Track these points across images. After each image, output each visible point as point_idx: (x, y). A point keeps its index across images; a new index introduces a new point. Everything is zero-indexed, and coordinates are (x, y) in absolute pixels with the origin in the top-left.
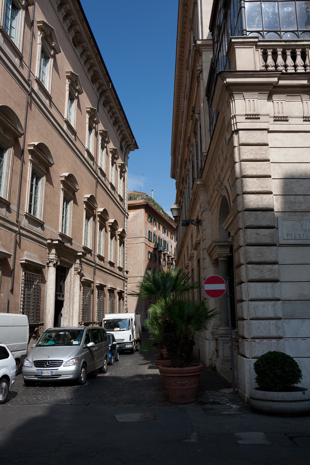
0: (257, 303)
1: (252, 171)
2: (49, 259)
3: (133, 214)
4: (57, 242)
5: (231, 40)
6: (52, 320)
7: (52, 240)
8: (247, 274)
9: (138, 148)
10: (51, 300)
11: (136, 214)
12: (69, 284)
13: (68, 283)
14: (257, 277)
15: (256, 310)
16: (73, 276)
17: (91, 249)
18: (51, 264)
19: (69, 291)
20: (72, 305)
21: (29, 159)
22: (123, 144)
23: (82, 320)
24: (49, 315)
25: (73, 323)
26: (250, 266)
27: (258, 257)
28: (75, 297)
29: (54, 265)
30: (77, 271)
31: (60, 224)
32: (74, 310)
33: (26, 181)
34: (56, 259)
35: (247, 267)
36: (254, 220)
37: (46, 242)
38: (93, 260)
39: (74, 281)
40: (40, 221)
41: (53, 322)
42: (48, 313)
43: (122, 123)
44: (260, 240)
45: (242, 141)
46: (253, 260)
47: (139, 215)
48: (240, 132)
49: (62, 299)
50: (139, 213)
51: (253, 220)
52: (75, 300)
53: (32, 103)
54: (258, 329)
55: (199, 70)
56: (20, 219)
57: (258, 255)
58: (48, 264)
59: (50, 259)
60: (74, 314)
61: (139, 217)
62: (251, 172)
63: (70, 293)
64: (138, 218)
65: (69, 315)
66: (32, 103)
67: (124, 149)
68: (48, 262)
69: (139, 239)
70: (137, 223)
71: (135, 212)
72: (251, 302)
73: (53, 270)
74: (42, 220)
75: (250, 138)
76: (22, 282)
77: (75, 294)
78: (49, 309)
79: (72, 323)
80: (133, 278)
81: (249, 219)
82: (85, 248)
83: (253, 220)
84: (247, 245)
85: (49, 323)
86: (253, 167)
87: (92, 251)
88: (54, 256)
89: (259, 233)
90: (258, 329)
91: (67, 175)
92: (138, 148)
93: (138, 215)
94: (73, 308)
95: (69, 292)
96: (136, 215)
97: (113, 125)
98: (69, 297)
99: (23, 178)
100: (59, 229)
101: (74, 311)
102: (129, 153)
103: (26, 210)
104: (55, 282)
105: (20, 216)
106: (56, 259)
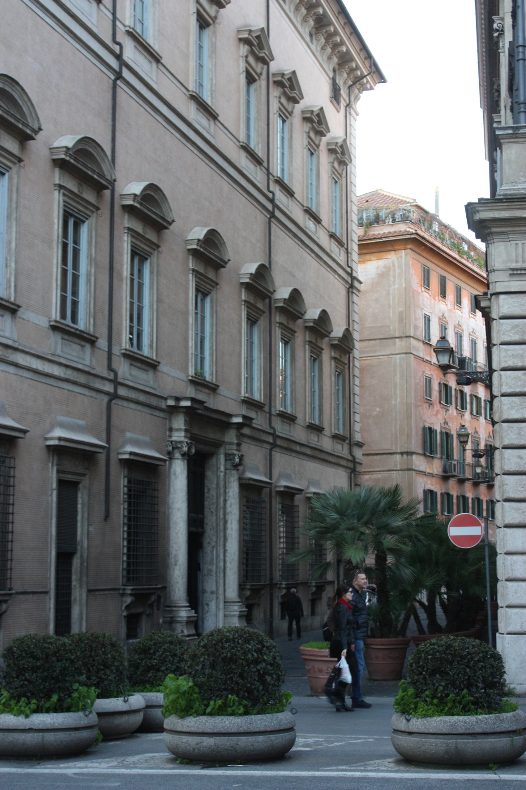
0: (515, 557)
1: (515, 361)
2: (172, 442)
3: (378, 268)
4: (188, 403)
5: (495, 132)
6: (182, 578)
7: (178, 399)
8: (502, 516)
9: (385, 81)
10: (179, 534)
11: (385, 267)
12: (215, 495)
13: (211, 492)
14: (516, 521)
15: (513, 568)
16: (222, 474)
17: (262, 401)
18: (177, 455)
19: (213, 510)
20: (221, 543)
21: (124, 228)
22: (340, 82)
23: (125, 580)
24: (177, 567)
25: (227, 587)
26: (507, 504)
27: (519, 491)
28: (229, 525)
29: (183, 455)
30: (233, 461)
31: (190, 355)
32: (228, 555)
33: (121, 279)
34: (187, 442)
35: (503, 505)
36: (516, 436)
37: (163, 406)
38: (268, 427)
39: (225, 487)
40: (152, 360)
41: (186, 584)
42: (174, 563)
43: (337, 24)
44: (524, 466)
45: (503, 313)
46: (512, 495)
47: (394, 270)
48: (502, 297)
49: (200, 530)
50: (394, 265)
51: (514, 437)
52: (229, 531)
53: (95, 23)
54: (516, 593)
55: (497, 31)
56: (114, 366)
57: (519, 489)
58: (169, 453)
59: (174, 443)
60: (228, 565)
61: (394, 277)
62: (514, 363)
63: (216, 515)
64: (392, 279)
65: (217, 567)
66: (95, 23)
67: (344, 93)
68: (170, 448)
69: (395, 344)
70: (388, 294)
71: (381, 263)
72: (506, 556)
73: (183, 467)
74: (155, 358)
75: (515, 307)
76: (124, 498)
77: (229, 518)
78: (176, 556)
79: (224, 585)
80: (379, 457)
81: (508, 434)
82: (249, 403)
83: (514, 437)
84: (504, 474)
85: (177, 585)
86: (518, 354)
87: (265, 405)
88: (183, 434)
89: (522, 456)
90: (516, 593)
91: (201, 237)
92: (385, 81)
93: (392, 269)
94: (225, 551)
95: (215, 513)
96: (384, 270)
97: (311, 35)
98: (215, 525)
99: (115, 274)
100: (190, 369)
101: (227, 559)
102: (357, 98)
103: (125, 344)
104: (187, 494)
105: (114, 358)
106: (187, 442)
